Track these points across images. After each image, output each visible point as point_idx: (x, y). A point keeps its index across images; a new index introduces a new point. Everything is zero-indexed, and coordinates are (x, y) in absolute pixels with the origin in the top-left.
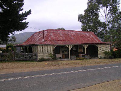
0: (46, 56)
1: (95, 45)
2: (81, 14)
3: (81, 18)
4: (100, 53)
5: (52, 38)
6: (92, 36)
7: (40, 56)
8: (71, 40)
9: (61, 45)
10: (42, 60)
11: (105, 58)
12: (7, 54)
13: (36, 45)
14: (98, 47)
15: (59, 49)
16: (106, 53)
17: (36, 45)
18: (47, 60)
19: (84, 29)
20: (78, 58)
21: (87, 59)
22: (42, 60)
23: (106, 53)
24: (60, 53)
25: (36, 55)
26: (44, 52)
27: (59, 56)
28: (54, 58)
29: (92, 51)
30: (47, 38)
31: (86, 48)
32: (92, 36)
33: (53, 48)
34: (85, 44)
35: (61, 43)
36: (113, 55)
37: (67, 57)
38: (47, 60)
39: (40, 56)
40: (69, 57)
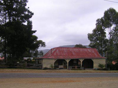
0: (49, 67)
1: (91, 59)
2: (90, 33)
3: (90, 37)
4: (96, 65)
5: (57, 54)
6: (93, 52)
7: (44, 66)
8: (72, 55)
9: (60, 59)
10: (46, 69)
11: (98, 69)
12: (22, 64)
13: (42, 59)
14: (94, 61)
15: (60, 62)
16: (101, 66)
17: (42, 59)
18: (50, 69)
19: (92, 46)
20: (73, 68)
21: (81, 69)
22: (46, 69)
23: (101, 66)
24: (62, 65)
25: (41, 66)
26: (47, 63)
27: (60, 66)
28: (56, 67)
29: (88, 64)
30: (53, 54)
31: (68, 62)
32: (93, 52)
33: (54, 61)
34: (81, 58)
35: (61, 58)
36: (109, 67)
37: (65, 67)
38: (50, 69)
39: (44, 66)
40: (67, 68)
